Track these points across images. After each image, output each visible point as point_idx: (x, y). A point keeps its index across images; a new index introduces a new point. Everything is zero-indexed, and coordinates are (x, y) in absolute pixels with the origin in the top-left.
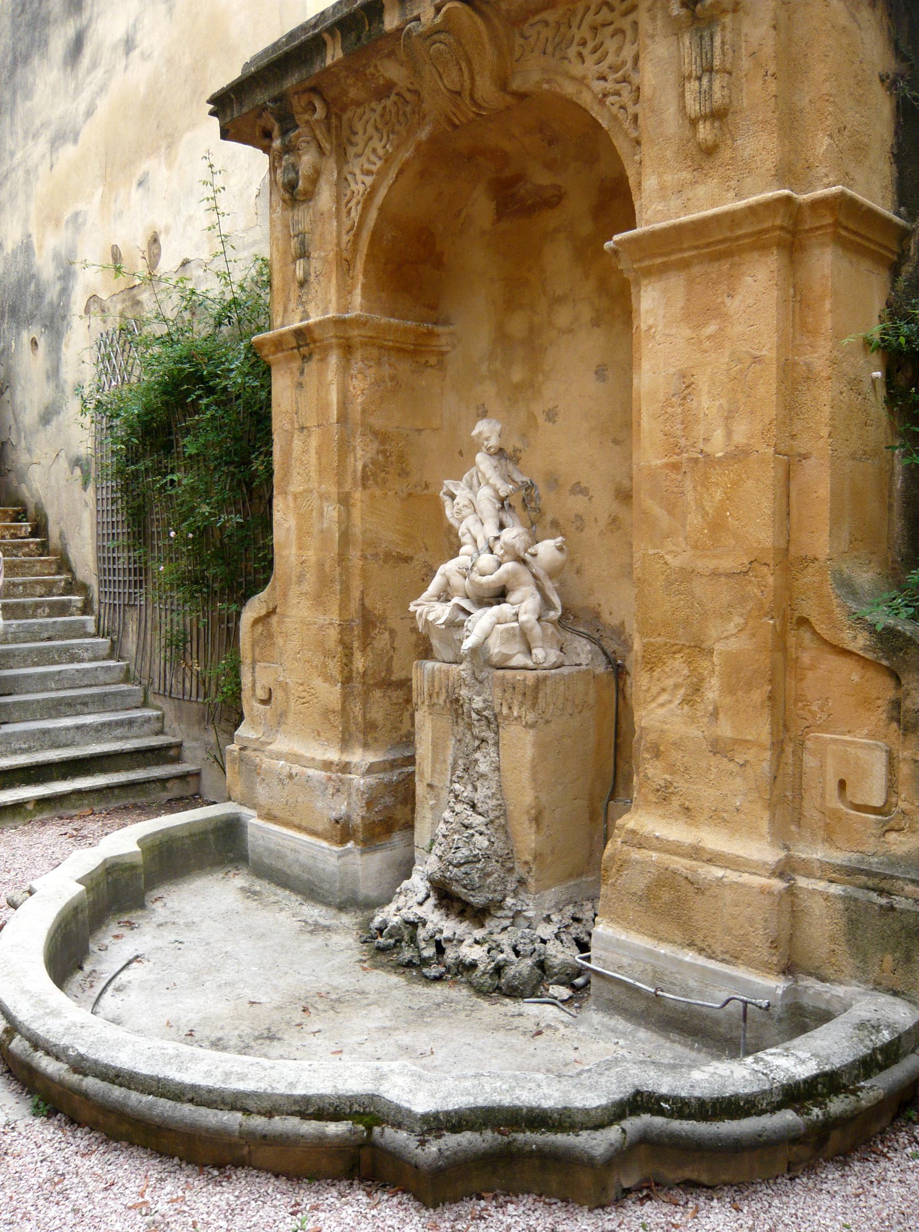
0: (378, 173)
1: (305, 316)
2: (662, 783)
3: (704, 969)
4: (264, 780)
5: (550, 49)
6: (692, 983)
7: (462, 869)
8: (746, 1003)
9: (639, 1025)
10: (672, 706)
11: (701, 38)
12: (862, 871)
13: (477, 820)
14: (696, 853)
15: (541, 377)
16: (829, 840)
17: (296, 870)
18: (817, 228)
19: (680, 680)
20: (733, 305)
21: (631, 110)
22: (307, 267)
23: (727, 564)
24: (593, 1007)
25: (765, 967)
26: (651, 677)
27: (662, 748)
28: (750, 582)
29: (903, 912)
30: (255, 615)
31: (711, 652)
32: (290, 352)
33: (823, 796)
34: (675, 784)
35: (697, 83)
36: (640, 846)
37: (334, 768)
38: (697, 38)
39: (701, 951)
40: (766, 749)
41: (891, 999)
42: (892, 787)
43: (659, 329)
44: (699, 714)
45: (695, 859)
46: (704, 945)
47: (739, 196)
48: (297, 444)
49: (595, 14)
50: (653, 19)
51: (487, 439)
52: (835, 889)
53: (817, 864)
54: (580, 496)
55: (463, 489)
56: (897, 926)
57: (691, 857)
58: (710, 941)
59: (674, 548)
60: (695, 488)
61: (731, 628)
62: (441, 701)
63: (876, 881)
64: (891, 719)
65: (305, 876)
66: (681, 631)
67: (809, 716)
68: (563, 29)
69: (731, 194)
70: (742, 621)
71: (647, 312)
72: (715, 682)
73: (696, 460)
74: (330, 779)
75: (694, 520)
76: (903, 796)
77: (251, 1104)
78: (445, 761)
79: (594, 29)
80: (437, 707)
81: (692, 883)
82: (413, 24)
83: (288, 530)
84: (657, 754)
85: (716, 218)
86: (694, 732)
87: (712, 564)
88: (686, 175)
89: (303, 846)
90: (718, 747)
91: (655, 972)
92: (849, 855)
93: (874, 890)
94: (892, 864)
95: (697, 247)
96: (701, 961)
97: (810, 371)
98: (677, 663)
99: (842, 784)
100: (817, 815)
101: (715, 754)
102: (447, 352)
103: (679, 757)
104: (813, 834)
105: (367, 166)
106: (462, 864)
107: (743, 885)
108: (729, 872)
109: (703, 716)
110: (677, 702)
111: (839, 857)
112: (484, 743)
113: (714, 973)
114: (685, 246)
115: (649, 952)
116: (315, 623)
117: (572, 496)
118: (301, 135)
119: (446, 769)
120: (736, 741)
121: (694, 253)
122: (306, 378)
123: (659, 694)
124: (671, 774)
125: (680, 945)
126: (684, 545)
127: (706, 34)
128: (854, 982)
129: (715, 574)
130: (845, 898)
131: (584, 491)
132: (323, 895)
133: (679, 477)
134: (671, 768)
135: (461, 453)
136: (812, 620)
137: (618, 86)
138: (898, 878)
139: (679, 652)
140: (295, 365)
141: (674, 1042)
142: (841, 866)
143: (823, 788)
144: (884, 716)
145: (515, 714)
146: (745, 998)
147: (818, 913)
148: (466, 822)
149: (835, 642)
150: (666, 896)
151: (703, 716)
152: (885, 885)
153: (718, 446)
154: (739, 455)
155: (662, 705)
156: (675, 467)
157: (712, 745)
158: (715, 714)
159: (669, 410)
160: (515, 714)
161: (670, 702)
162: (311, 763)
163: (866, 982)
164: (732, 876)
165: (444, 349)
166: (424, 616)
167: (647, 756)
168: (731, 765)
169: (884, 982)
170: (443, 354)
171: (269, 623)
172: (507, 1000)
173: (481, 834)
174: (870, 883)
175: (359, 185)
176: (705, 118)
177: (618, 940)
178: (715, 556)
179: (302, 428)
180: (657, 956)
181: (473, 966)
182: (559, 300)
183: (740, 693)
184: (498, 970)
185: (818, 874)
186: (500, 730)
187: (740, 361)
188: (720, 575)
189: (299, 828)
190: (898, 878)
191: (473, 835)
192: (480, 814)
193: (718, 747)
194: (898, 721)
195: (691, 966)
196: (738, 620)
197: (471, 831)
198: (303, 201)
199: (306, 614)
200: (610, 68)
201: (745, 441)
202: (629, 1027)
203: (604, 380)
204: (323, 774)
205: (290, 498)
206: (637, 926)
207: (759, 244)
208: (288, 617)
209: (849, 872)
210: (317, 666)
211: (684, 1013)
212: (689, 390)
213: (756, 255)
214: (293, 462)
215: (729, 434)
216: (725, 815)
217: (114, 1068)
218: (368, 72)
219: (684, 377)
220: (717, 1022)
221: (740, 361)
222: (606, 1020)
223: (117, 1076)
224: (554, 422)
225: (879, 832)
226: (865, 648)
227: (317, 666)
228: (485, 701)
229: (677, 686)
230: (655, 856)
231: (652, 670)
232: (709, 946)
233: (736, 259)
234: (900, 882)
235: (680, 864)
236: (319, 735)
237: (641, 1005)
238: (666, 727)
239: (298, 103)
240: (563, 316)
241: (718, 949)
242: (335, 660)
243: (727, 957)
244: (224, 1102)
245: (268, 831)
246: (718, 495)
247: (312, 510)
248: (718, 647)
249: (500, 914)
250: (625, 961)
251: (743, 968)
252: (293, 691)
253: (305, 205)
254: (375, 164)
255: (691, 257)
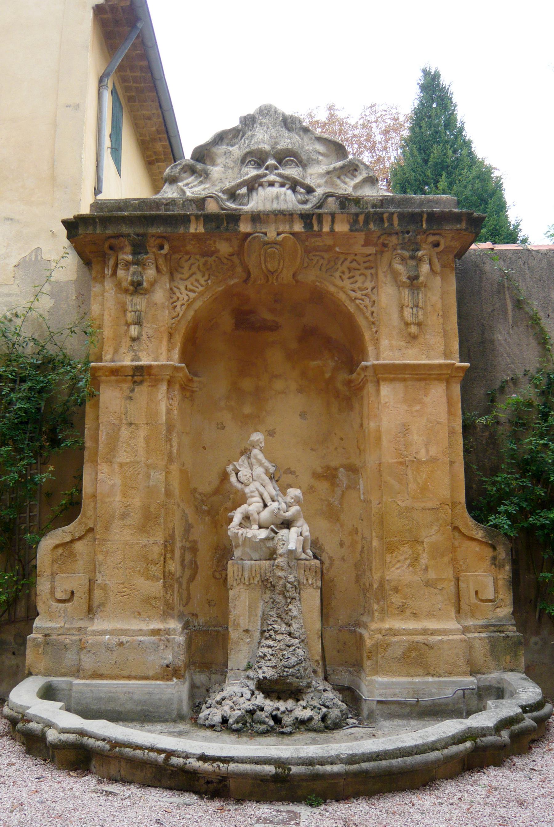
0: (199, 293)
1: (136, 358)
2: (400, 604)
3: (439, 681)
4: (89, 651)
5: (324, 269)
6: (434, 691)
7: (296, 668)
8: (463, 690)
9: (409, 719)
10: (403, 568)
11: (413, 293)
12: (491, 626)
13: (296, 641)
14: (425, 632)
15: (264, 413)
16: (473, 616)
17: (129, 706)
18: (457, 377)
19: (407, 556)
20: (427, 400)
21: (370, 309)
22: (140, 331)
23: (429, 505)
24: (382, 720)
25: (464, 674)
26: (392, 556)
27: (399, 588)
28: (440, 512)
29: (512, 637)
30: (57, 542)
31: (423, 542)
32: (124, 378)
33: (469, 599)
34: (408, 604)
35: (411, 310)
36: (395, 635)
37: (161, 633)
38: (411, 292)
39: (433, 675)
40: (451, 581)
41: (512, 673)
42: (496, 592)
43: (391, 404)
44: (418, 570)
45: (424, 635)
46: (435, 673)
47: (428, 358)
48: (124, 433)
49: (351, 263)
50: (386, 277)
51: (261, 443)
52: (483, 635)
53: (473, 627)
54: (290, 475)
55: (246, 468)
56: (510, 643)
57: (422, 634)
58: (438, 670)
59: (402, 498)
60: (412, 473)
61: (433, 532)
62: (256, 582)
63: (498, 628)
64: (492, 564)
65: (139, 708)
66: (407, 534)
67: (459, 567)
68: (332, 263)
69: (424, 356)
70: (437, 528)
71: (384, 396)
72: (425, 555)
73: (413, 461)
74: (161, 640)
75: (413, 486)
76: (501, 593)
77: (438, 745)
78: (256, 615)
79: (349, 269)
80: (253, 585)
81: (427, 645)
82: (261, 234)
83: (113, 485)
84: (396, 590)
85: (424, 365)
86: (417, 578)
87: (423, 505)
88: (403, 344)
89: (138, 688)
90: (428, 584)
91: (414, 691)
92: (483, 620)
93: (497, 632)
94: (500, 621)
95: (411, 374)
96: (437, 679)
97: (453, 430)
98: (405, 549)
99: (477, 593)
100: (467, 607)
101: (427, 586)
102: (196, 391)
103: (409, 591)
104: (466, 615)
105: (190, 287)
106: (294, 666)
107: (453, 640)
108: (443, 637)
109: (420, 571)
110: (406, 566)
111: (480, 622)
112: (294, 600)
113: (445, 682)
114: (407, 373)
115: (410, 683)
116: (138, 544)
117: (285, 475)
118: (149, 258)
119: (258, 620)
120: (437, 580)
121: (410, 376)
122: (136, 394)
123: (396, 564)
124: (405, 599)
125: (422, 675)
126: (408, 497)
127: (415, 292)
128: (495, 671)
129: (424, 509)
130: (489, 637)
131: (293, 473)
132: (159, 716)
133: (404, 468)
134: (405, 597)
135: (204, 448)
136: (460, 528)
137: (363, 297)
138: (506, 625)
139: (406, 544)
140: (126, 386)
141: (429, 721)
142: (483, 625)
143: (469, 595)
144: (489, 563)
145: (310, 582)
146: (462, 688)
147: (477, 646)
148: (289, 643)
149: (469, 536)
150: (413, 655)
151: (420, 571)
152: (501, 629)
153: (423, 455)
154: (433, 460)
155: (398, 569)
156: (401, 463)
157: (426, 583)
158: (426, 569)
159: (397, 439)
160: (310, 582)
161: (402, 566)
162: (141, 632)
163: (500, 670)
164: (445, 638)
165: (194, 389)
166: (244, 535)
167: (391, 593)
168: (436, 590)
169: (507, 667)
170: (193, 392)
171: (71, 547)
172: (334, 731)
173: (298, 648)
174: (495, 629)
175: (183, 296)
176: (414, 324)
177: (392, 682)
178: (423, 501)
179: (131, 424)
180: (415, 683)
181: (311, 719)
182: (277, 376)
183: (438, 559)
184: (324, 718)
185: (473, 631)
186: (302, 592)
187: (431, 422)
188: (426, 509)
189: (129, 677)
190: (506, 625)
191: (294, 650)
192: (296, 638)
193: (428, 584)
194: (495, 564)
195: (432, 682)
196: (435, 528)
197: (294, 648)
198: (142, 294)
199: (129, 538)
200: (358, 288)
201: (435, 455)
202: (405, 722)
203: (305, 419)
204: (153, 638)
205: (116, 467)
206: (398, 673)
207: (439, 378)
208: (109, 540)
209: (486, 627)
210: (139, 571)
211: (431, 706)
212: (407, 431)
213: (436, 382)
214: (120, 444)
215: (427, 451)
216: (434, 613)
217: (375, 752)
218: (208, 242)
219: (405, 426)
220: (447, 705)
221: (431, 422)
222: (391, 723)
223: (378, 756)
224: (273, 437)
225: (493, 609)
226: (482, 537)
227: (139, 571)
228: (295, 577)
229: (405, 559)
230: (405, 638)
231: (392, 553)
232: (437, 672)
233: (428, 382)
234: (507, 626)
235: (419, 638)
236: (139, 614)
237: (408, 709)
238: (401, 578)
239: (152, 243)
240: (279, 385)
241: (441, 672)
242: (158, 565)
243: (446, 674)
244: (429, 749)
245: (95, 686)
246: (424, 476)
247: (138, 474)
248: (426, 540)
249: (309, 690)
250: (397, 691)
251: (455, 677)
252: (112, 589)
253: (143, 296)
254: (198, 288)
255: (408, 377)
